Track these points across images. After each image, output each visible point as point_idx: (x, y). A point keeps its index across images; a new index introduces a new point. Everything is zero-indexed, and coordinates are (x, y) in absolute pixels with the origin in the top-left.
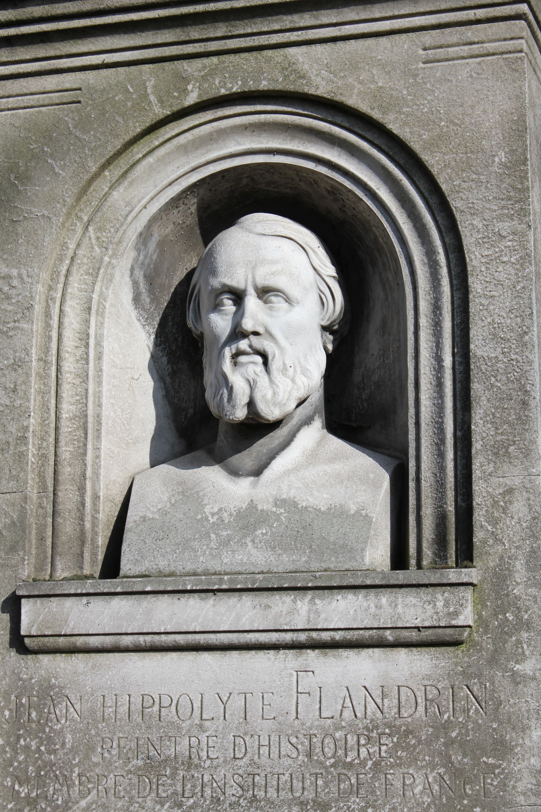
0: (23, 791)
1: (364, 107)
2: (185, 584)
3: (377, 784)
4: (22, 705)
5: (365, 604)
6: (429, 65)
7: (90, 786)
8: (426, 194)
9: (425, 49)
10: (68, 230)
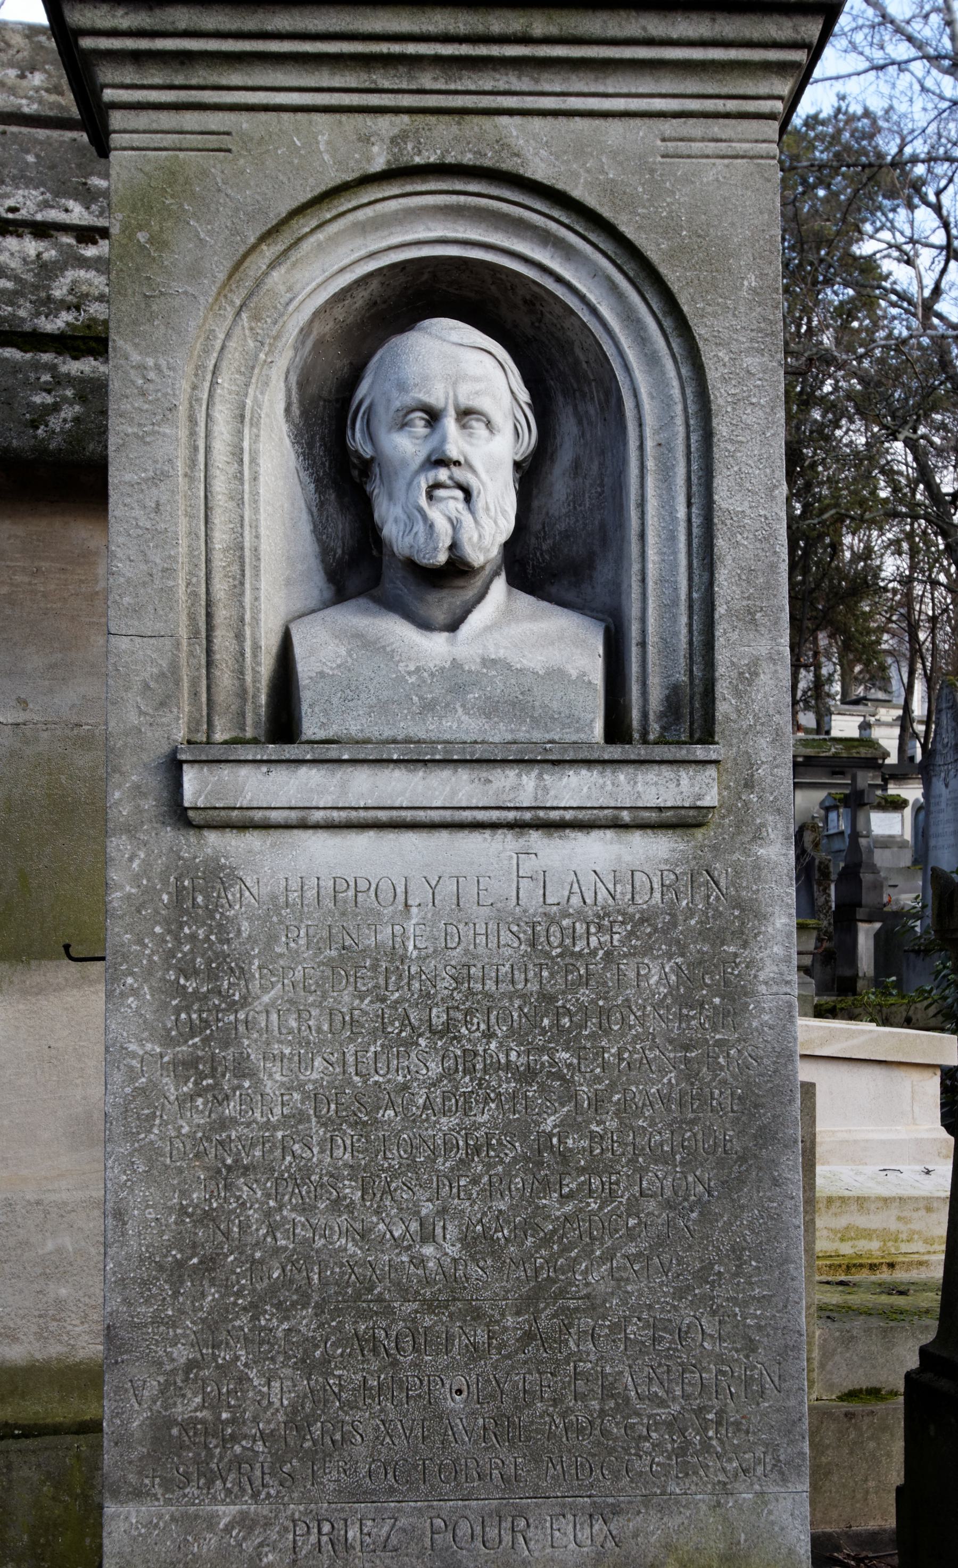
0: (191, 986)
1: (591, 201)
2: (390, 753)
3: (609, 975)
4: (184, 888)
5: (601, 781)
6: (668, 160)
7: (273, 979)
8: (660, 316)
9: (663, 140)
10: (215, 315)
